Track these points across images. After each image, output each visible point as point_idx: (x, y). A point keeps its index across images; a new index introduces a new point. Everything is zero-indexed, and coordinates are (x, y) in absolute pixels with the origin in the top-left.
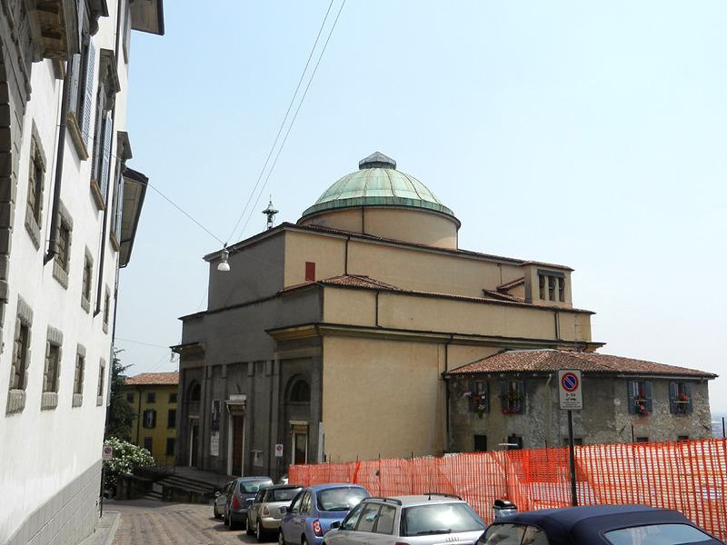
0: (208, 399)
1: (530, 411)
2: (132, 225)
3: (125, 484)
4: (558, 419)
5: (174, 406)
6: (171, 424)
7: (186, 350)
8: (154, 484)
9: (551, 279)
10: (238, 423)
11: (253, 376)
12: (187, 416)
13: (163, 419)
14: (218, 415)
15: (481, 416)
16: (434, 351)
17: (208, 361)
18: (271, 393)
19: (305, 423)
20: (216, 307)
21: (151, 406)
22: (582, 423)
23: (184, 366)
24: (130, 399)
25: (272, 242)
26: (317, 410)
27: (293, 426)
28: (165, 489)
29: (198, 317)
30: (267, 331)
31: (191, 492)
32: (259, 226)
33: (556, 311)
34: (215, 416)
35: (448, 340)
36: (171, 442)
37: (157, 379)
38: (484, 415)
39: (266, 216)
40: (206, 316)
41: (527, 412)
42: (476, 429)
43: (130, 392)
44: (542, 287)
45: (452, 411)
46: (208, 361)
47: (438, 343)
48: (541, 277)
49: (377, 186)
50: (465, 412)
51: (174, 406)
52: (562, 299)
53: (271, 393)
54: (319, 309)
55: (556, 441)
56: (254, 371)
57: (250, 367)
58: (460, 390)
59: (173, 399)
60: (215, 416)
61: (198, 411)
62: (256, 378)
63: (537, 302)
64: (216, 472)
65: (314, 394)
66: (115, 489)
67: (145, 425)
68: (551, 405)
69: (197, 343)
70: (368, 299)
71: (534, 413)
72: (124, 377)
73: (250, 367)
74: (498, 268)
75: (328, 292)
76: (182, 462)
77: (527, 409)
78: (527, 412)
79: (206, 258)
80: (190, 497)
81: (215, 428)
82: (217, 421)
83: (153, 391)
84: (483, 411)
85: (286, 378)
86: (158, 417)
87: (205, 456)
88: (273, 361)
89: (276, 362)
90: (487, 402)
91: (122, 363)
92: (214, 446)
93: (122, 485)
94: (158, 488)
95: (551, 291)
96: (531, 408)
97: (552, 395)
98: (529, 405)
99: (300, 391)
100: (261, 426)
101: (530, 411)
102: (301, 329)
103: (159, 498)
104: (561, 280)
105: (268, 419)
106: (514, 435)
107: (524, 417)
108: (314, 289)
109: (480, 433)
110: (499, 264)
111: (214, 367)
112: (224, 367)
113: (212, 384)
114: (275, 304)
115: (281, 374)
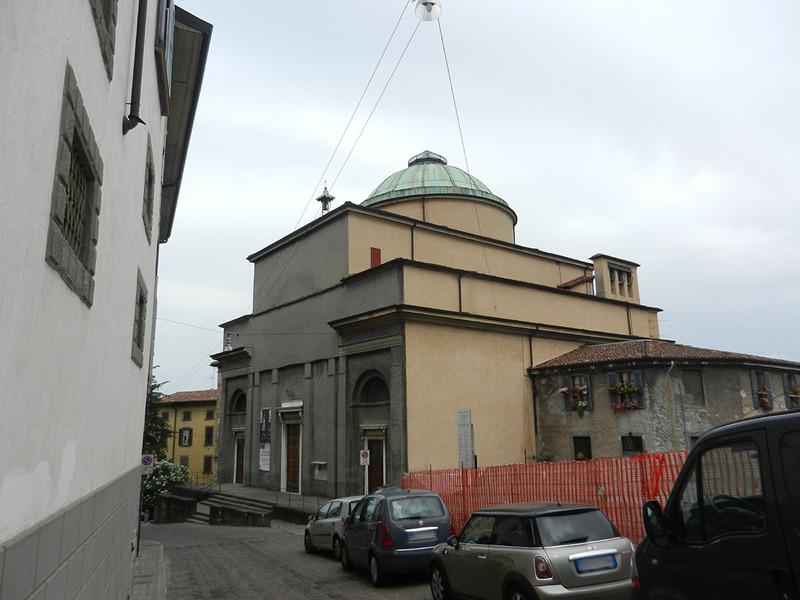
0: (255, 409)
1: (651, 405)
2: (180, 145)
3: (164, 506)
4: (683, 413)
5: (211, 423)
6: (209, 440)
7: (221, 361)
8: (198, 505)
9: (620, 273)
10: (293, 432)
11: (312, 378)
12: (230, 429)
13: (199, 436)
14: (268, 425)
15: (581, 415)
16: (519, 345)
17: (256, 366)
18: (336, 395)
19: (382, 426)
20: (264, 308)
21: (187, 424)
22: (709, 418)
23: (225, 376)
24: (166, 416)
25: (259, 312)
26: (400, 410)
27: (365, 431)
28: (213, 509)
29: (243, 321)
30: (331, 324)
31: (249, 513)
32: (315, 212)
33: (628, 306)
34: (264, 426)
35: (533, 332)
36: (208, 460)
37: (194, 396)
38: (586, 413)
39: (320, 204)
40: (251, 320)
41: (648, 406)
42: (574, 429)
43: (164, 410)
44: (612, 281)
45: (541, 410)
46: (256, 366)
47: (522, 335)
48: (612, 271)
49: (433, 179)
50: (558, 411)
51: (211, 423)
52: (631, 295)
53: (336, 395)
54: (398, 292)
55: (682, 440)
56: (312, 372)
57: (308, 368)
58: (551, 387)
59: (210, 416)
60: (264, 426)
61: (243, 422)
62: (315, 379)
63: (609, 296)
64: (268, 488)
65: (394, 392)
66: (151, 510)
67: (180, 443)
68: (673, 397)
69: (242, 348)
70: (450, 283)
71: (656, 408)
72: (160, 394)
73: (308, 368)
74: (557, 267)
75: (409, 274)
76: (225, 478)
77: (648, 402)
78: (648, 406)
79: (250, 258)
80: (247, 518)
81: (264, 438)
82: (266, 432)
83: (188, 409)
84: (584, 408)
85: (355, 377)
86: (194, 433)
87: (254, 470)
88: (337, 359)
89: (341, 359)
90: (589, 397)
91: (158, 380)
92: (264, 459)
93: (160, 506)
94: (203, 508)
95: (621, 285)
96: (652, 402)
97: (673, 386)
98: (650, 398)
99: (376, 390)
100: (324, 433)
101: (651, 405)
102: (376, 315)
103: (204, 520)
104: (629, 275)
105: (333, 425)
106: (630, 434)
107: (643, 412)
108: (386, 270)
109: (581, 434)
110: (558, 263)
111: (261, 373)
112: (275, 372)
113: (260, 393)
114: (338, 294)
115: (347, 373)
